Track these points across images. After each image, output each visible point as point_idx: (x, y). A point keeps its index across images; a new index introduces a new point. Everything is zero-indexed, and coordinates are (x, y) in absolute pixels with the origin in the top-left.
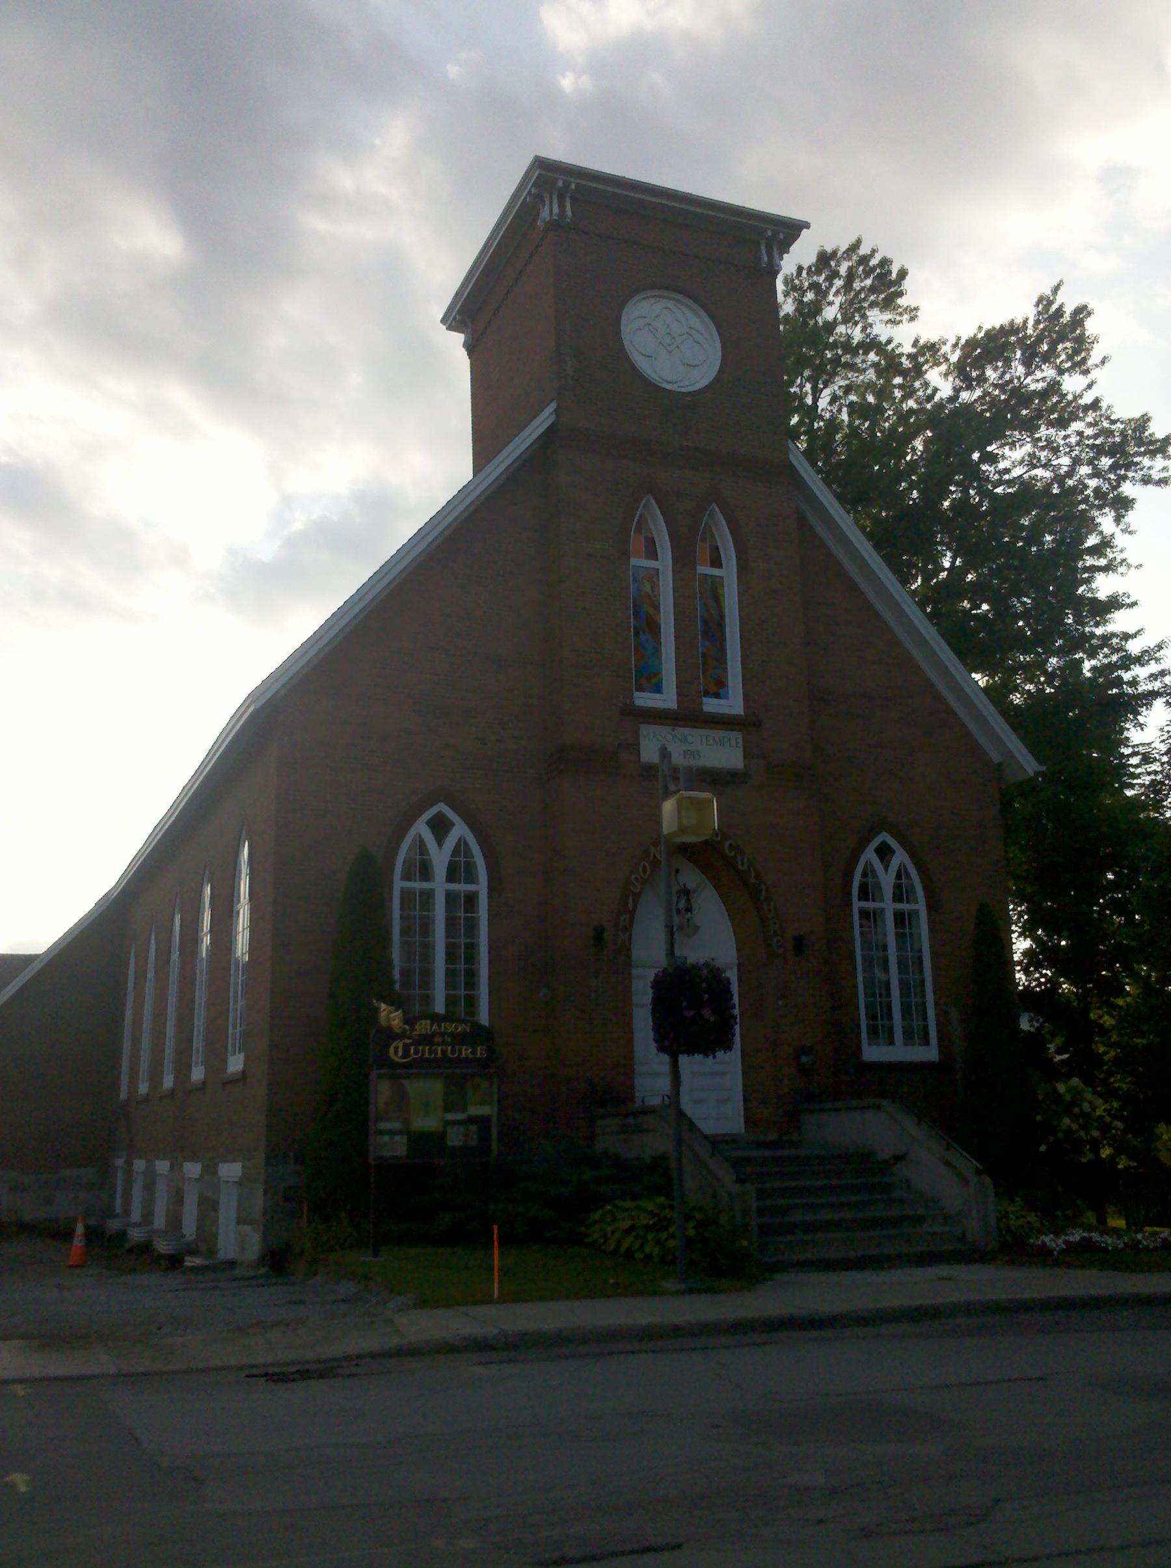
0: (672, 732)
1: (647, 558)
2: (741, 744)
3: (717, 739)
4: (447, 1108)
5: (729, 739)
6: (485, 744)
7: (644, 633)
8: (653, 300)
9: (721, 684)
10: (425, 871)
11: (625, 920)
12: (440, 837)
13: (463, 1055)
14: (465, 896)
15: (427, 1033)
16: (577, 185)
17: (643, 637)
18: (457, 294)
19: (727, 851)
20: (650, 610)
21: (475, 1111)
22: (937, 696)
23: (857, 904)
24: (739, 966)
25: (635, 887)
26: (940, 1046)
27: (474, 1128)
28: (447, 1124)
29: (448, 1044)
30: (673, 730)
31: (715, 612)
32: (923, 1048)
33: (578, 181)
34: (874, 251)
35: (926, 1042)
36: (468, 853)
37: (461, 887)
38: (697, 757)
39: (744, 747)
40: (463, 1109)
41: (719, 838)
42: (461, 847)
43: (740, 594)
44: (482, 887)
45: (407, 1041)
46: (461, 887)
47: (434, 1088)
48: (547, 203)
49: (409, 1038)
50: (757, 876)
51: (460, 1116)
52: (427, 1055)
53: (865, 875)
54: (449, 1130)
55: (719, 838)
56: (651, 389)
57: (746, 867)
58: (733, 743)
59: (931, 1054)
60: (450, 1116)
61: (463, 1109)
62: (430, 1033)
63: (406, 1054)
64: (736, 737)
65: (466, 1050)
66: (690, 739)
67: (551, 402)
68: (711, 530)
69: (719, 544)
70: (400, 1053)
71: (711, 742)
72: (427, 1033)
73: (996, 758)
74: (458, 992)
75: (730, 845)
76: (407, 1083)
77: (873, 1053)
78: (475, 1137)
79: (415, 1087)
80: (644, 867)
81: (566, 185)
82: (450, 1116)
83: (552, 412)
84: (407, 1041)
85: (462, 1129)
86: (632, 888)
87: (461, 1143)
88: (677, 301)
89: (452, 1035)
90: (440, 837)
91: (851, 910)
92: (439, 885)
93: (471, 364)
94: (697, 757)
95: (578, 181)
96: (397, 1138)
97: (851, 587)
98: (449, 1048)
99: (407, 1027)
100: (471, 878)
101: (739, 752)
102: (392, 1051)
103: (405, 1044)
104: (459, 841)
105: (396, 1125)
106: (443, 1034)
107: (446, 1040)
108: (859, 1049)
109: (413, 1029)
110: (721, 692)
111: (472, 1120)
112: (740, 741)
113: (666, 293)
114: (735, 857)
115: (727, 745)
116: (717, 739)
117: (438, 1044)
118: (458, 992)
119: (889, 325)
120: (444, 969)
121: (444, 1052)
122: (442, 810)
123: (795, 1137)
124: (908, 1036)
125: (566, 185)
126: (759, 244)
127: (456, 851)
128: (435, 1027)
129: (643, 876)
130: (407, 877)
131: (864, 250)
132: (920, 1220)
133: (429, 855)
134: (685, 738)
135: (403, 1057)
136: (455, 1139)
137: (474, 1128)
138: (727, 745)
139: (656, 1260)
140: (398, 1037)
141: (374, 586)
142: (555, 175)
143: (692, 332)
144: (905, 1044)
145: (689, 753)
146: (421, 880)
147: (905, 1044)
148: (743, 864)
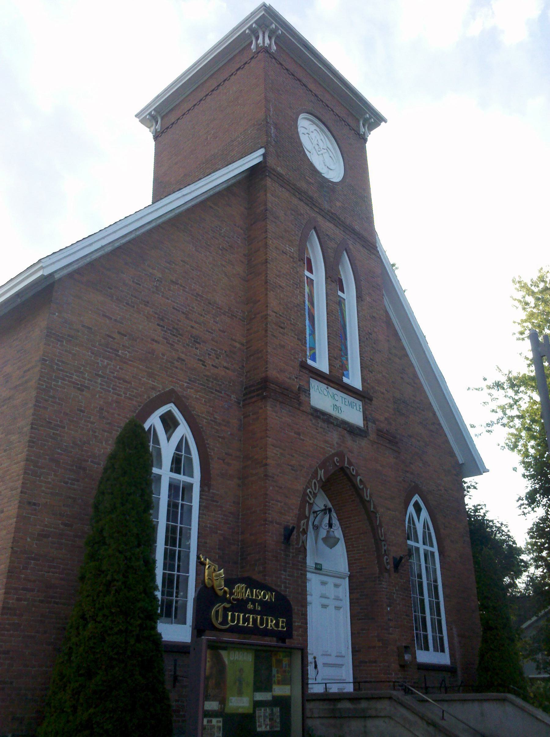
0: (327, 390)
2: (361, 410)
4: (257, 688)
6: (205, 366)
13: (269, 627)
15: (242, 599)
18: (158, 96)
24: (350, 577)
27: (277, 710)
28: (257, 704)
29: (258, 613)
30: (327, 388)
32: (440, 654)
35: (443, 650)
40: (270, 690)
42: (182, 445)
44: (196, 480)
45: (228, 606)
49: (229, 601)
50: (374, 507)
60: (260, 696)
62: (245, 598)
65: (272, 621)
67: (261, 148)
69: (343, 278)
70: (220, 619)
71: (347, 403)
72: (242, 599)
73: (461, 460)
74: (174, 573)
80: (315, 483)
82: (260, 696)
83: (260, 156)
84: (228, 606)
87: (268, 728)
88: (320, 128)
89: (262, 603)
94: (340, 411)
96: (214, 721)
103: (224, 608)
104: (183, 437)
106: (254, 602)
107: (257, 609)
118: (174, 573)
120: (164, 549)
121: (255, 621)
125: (277, 29)
129: (314, 491)
135: (221, 624)
137: (277, 710)
148: (367, 497)
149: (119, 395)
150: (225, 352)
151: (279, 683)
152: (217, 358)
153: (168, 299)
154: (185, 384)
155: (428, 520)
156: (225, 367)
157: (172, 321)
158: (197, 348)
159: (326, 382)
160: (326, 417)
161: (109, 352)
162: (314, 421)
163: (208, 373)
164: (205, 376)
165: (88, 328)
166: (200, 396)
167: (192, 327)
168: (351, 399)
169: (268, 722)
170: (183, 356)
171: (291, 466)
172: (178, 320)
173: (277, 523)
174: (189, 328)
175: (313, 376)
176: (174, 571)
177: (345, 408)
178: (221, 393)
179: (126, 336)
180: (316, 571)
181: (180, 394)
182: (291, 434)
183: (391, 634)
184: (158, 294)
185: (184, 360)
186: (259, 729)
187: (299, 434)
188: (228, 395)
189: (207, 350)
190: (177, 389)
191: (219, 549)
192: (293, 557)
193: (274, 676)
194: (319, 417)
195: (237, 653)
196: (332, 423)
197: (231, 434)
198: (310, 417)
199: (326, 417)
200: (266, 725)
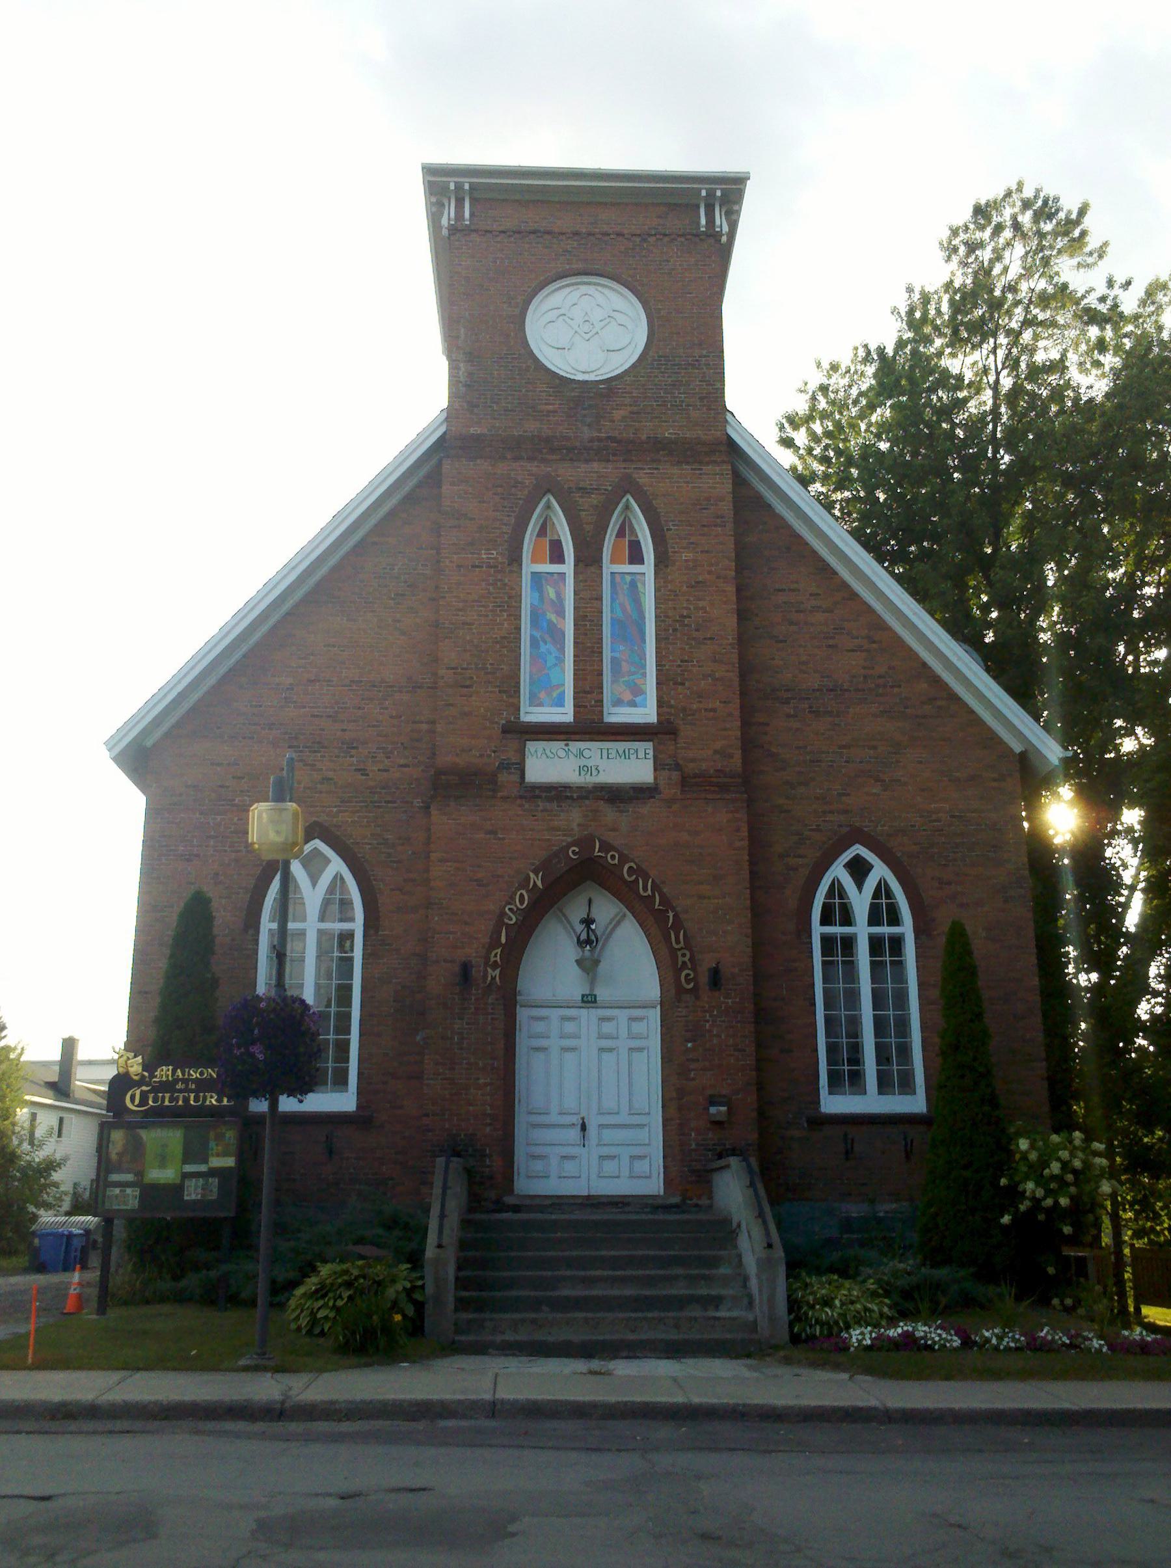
1: (552, 561)
3: (621, 752)
4: (185, 1161)
5: (637, 751)
6: (367, 775)
7: (545, 643)
8: (568, 290)
9: (638, 691)
10: (844, 915)
11: (496, 955)
12: (859, 880)
14: (841, 938)
16: (722, 190)
17: (543, 648)
19: (626, 875)
20: (553, 617)
21: (216, 1162)
22: (936, 681)
23: (818, 930)
25: (511, 919)
26: (359, 1093)
27: (214, 1182)
28: (185, 1176)
29: (192, 1091)
30: (567, 745)
31: (635, 616)
33: (456, 179)
34: (1038, 191)
36: (889, 894)
37: (885, 930)
38: (595, 773)
39: (655, 757)
40: (206, 1161)
41: (616, 861)
42: (882, 890)
43: (657, 590)
45: (144, 1088)
46: (885, 930)
47: (172, 1138)
48: (447, 208)
51: (203, 1168)
52: (167, 1103)
53: (830, 893)
54: (187, 1183)
55: (616, 861)
56: (560, 383)
57: (649, 892)
58: (641, 754)
59: (916, 1103)
60: (189, 1168)
61: (206, 1161)
63: (143, 1102)
64: (646, 748)
66: (586, 753)
68: (551, 519)
70: (137, 1102)
73: (1018, 748)
75: (630, 868)
76: (144, 1134)
77: (834, 1104)
78: (215, 1190)
79: (151, 1137)
81: (711, 194)
82: (189, 1168)
84: (144, 1088)
85: (201, 1181)
86: (506, 921)
87: (199, 1197)
89: (196, 1081)
90: (859, 880)
91: (810, 936)
92: (862, 931)
93: (723, 397)
95: (456, 179)
96: (129, 1191)
97: (826, 570)
98: (192, 1096)
99: (146, 1074)
100: (895, 920)
101: (649, 764)
102: (128, 1097)
104: (336, 875)
105: (129, 1177)
108: (817, 1102)
109: (152, 1076)
110: (638, 699)
111: (213, 1172)
112: (651, 752)
113: (585, 279)
114: (636, 880)
115: (633, 757)
116: (621, 752)
117: (180, 1091)
119: (1082, 270)
121: (186, 1100)
122: (860, 853)
123: (704, 1201)
124: (884, 1085)
125: (459, 187)
126: (698, 207)
127: (877, 894)
128: (179, 1072)
130: (826, 920)
131: (1028, 193)
132: (716, 1301)
133: (848, 898)
134: (581, 753)
136: (193, 1192)
138: (633, 757)
139: (304, 1332)
140: (139, 1084)
141: (237, 624)
142: (713, 186)
143: (614, 314)
144: (880, 1093)
145: (586, 769)
146: (889, 925)
147: (880, 1093)
149: (239, 851)
150: (402, 744)
151: (218, 1155)
152: (388, 758)
153: (305, 707)
154: (335, 809)
155: (889, 882)
156: (402, 766)
157: (311, 734)
158: (352, 756)
159: (563, 737)
160: (553, 793)
161: (223, 805)
162: (527, 806)
163: (371, 783)
164: (367, 788)
165: (194, 786)
166: (359, 817)
167: (343, 730)
168: (621, 746)
169: (199, 1190)
170: (330, 774)
171: (476, 880)
172: (321, 730)
173: (445, 961)
174: (339, 733)
175: (527, 736)
176: (329, 1035)
177: (603, 764)
178: (395, 802)
179: (243, 778)
180: (583, 1005)
181: (326, 824)
182: (477, 836)
183: (693, 1079)
184: (289, 707)
185: (331, 779)
186: (186, 1198)
187: (493, 832)
188: (407, 802)
189: (369, 752)
190: (323, 818)
191: (394, 1001)
192: (477, 999)
193: (212, 1149)
194: (539, 797)
195: (159, 1130)
196: (571, 798)
197: (414, 853)
198: (518, 802)
199: (553, 793)
200: (197, 1194)
